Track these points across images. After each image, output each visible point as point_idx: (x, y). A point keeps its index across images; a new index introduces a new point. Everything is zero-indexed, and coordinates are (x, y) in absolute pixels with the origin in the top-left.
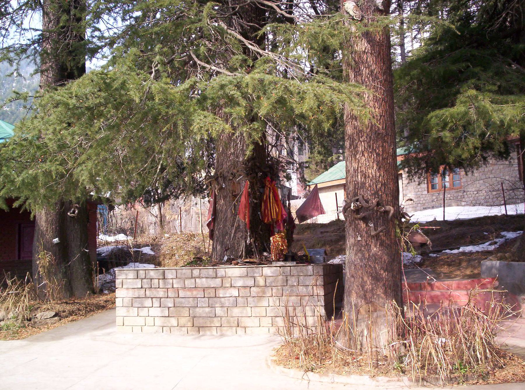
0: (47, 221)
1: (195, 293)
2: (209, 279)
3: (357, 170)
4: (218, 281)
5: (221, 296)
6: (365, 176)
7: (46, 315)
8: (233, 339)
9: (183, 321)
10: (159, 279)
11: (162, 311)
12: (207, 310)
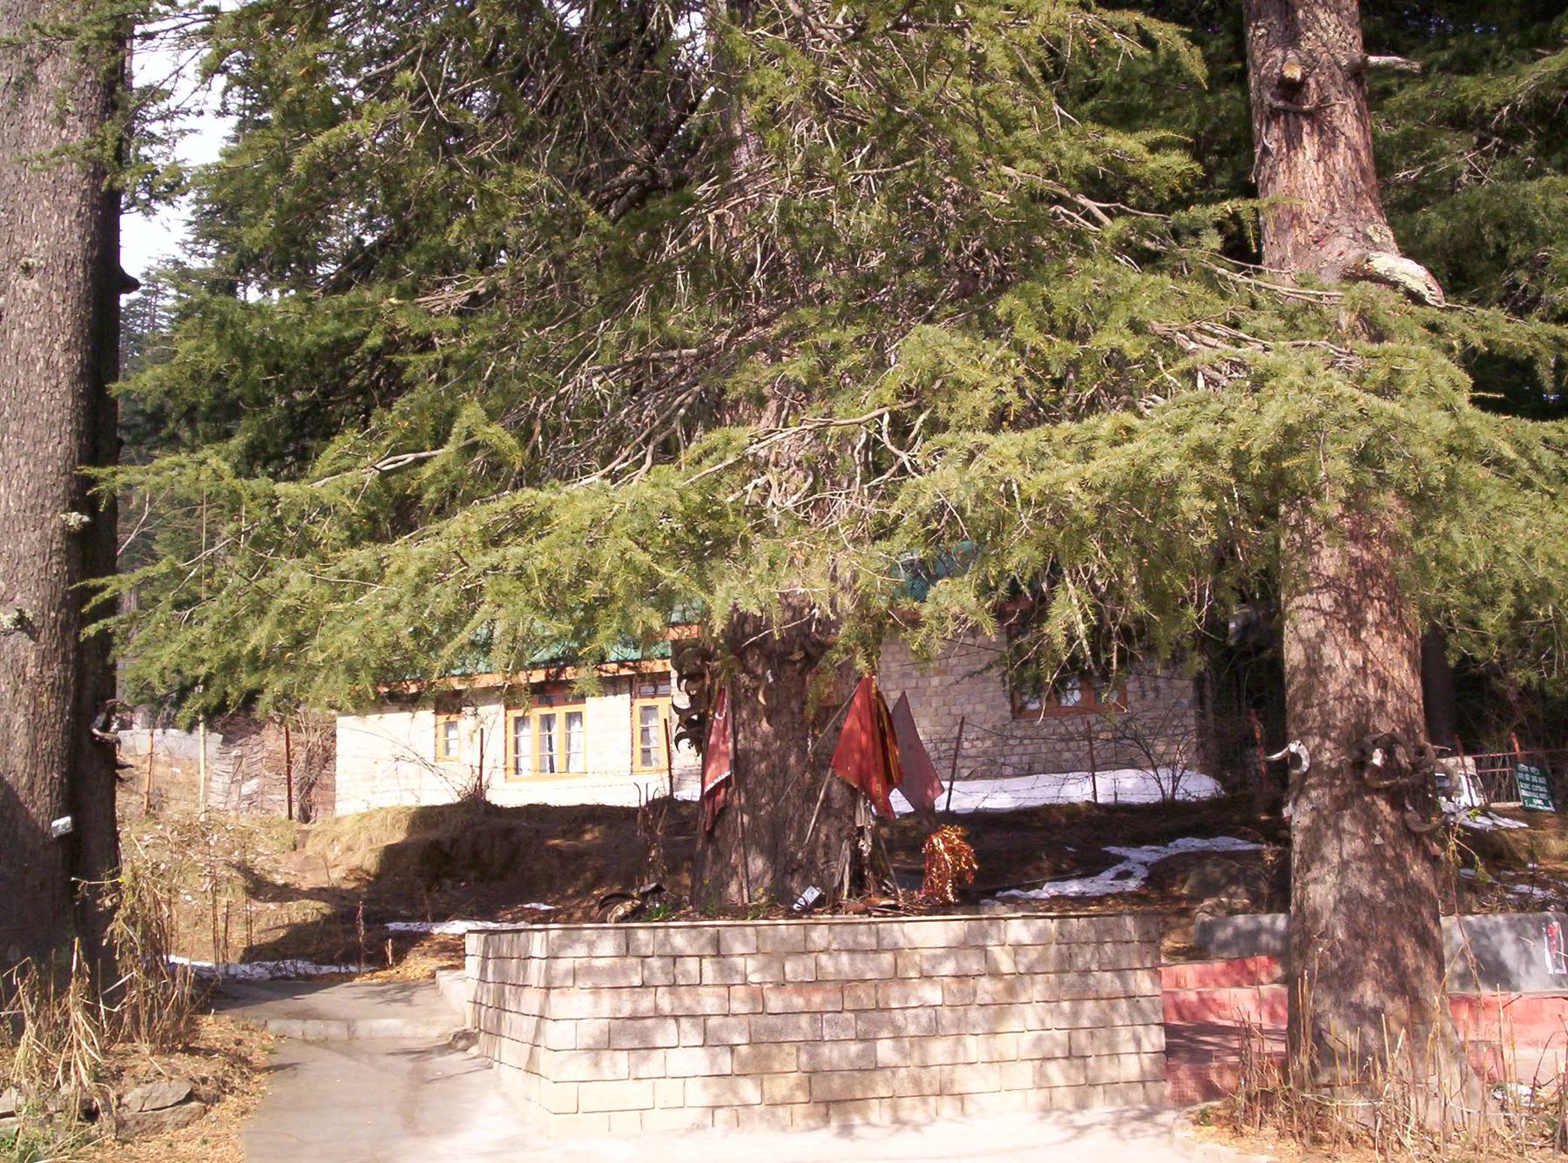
1: (817, 999)
2: (859, 957)
3: (1364, 668)
4: (887, 958)
5: (894, 1005)
6: (1383, 684)
8: (943, 1131)
9: (780, 1087)
11: (713, 1060)
12: (854, 1048)
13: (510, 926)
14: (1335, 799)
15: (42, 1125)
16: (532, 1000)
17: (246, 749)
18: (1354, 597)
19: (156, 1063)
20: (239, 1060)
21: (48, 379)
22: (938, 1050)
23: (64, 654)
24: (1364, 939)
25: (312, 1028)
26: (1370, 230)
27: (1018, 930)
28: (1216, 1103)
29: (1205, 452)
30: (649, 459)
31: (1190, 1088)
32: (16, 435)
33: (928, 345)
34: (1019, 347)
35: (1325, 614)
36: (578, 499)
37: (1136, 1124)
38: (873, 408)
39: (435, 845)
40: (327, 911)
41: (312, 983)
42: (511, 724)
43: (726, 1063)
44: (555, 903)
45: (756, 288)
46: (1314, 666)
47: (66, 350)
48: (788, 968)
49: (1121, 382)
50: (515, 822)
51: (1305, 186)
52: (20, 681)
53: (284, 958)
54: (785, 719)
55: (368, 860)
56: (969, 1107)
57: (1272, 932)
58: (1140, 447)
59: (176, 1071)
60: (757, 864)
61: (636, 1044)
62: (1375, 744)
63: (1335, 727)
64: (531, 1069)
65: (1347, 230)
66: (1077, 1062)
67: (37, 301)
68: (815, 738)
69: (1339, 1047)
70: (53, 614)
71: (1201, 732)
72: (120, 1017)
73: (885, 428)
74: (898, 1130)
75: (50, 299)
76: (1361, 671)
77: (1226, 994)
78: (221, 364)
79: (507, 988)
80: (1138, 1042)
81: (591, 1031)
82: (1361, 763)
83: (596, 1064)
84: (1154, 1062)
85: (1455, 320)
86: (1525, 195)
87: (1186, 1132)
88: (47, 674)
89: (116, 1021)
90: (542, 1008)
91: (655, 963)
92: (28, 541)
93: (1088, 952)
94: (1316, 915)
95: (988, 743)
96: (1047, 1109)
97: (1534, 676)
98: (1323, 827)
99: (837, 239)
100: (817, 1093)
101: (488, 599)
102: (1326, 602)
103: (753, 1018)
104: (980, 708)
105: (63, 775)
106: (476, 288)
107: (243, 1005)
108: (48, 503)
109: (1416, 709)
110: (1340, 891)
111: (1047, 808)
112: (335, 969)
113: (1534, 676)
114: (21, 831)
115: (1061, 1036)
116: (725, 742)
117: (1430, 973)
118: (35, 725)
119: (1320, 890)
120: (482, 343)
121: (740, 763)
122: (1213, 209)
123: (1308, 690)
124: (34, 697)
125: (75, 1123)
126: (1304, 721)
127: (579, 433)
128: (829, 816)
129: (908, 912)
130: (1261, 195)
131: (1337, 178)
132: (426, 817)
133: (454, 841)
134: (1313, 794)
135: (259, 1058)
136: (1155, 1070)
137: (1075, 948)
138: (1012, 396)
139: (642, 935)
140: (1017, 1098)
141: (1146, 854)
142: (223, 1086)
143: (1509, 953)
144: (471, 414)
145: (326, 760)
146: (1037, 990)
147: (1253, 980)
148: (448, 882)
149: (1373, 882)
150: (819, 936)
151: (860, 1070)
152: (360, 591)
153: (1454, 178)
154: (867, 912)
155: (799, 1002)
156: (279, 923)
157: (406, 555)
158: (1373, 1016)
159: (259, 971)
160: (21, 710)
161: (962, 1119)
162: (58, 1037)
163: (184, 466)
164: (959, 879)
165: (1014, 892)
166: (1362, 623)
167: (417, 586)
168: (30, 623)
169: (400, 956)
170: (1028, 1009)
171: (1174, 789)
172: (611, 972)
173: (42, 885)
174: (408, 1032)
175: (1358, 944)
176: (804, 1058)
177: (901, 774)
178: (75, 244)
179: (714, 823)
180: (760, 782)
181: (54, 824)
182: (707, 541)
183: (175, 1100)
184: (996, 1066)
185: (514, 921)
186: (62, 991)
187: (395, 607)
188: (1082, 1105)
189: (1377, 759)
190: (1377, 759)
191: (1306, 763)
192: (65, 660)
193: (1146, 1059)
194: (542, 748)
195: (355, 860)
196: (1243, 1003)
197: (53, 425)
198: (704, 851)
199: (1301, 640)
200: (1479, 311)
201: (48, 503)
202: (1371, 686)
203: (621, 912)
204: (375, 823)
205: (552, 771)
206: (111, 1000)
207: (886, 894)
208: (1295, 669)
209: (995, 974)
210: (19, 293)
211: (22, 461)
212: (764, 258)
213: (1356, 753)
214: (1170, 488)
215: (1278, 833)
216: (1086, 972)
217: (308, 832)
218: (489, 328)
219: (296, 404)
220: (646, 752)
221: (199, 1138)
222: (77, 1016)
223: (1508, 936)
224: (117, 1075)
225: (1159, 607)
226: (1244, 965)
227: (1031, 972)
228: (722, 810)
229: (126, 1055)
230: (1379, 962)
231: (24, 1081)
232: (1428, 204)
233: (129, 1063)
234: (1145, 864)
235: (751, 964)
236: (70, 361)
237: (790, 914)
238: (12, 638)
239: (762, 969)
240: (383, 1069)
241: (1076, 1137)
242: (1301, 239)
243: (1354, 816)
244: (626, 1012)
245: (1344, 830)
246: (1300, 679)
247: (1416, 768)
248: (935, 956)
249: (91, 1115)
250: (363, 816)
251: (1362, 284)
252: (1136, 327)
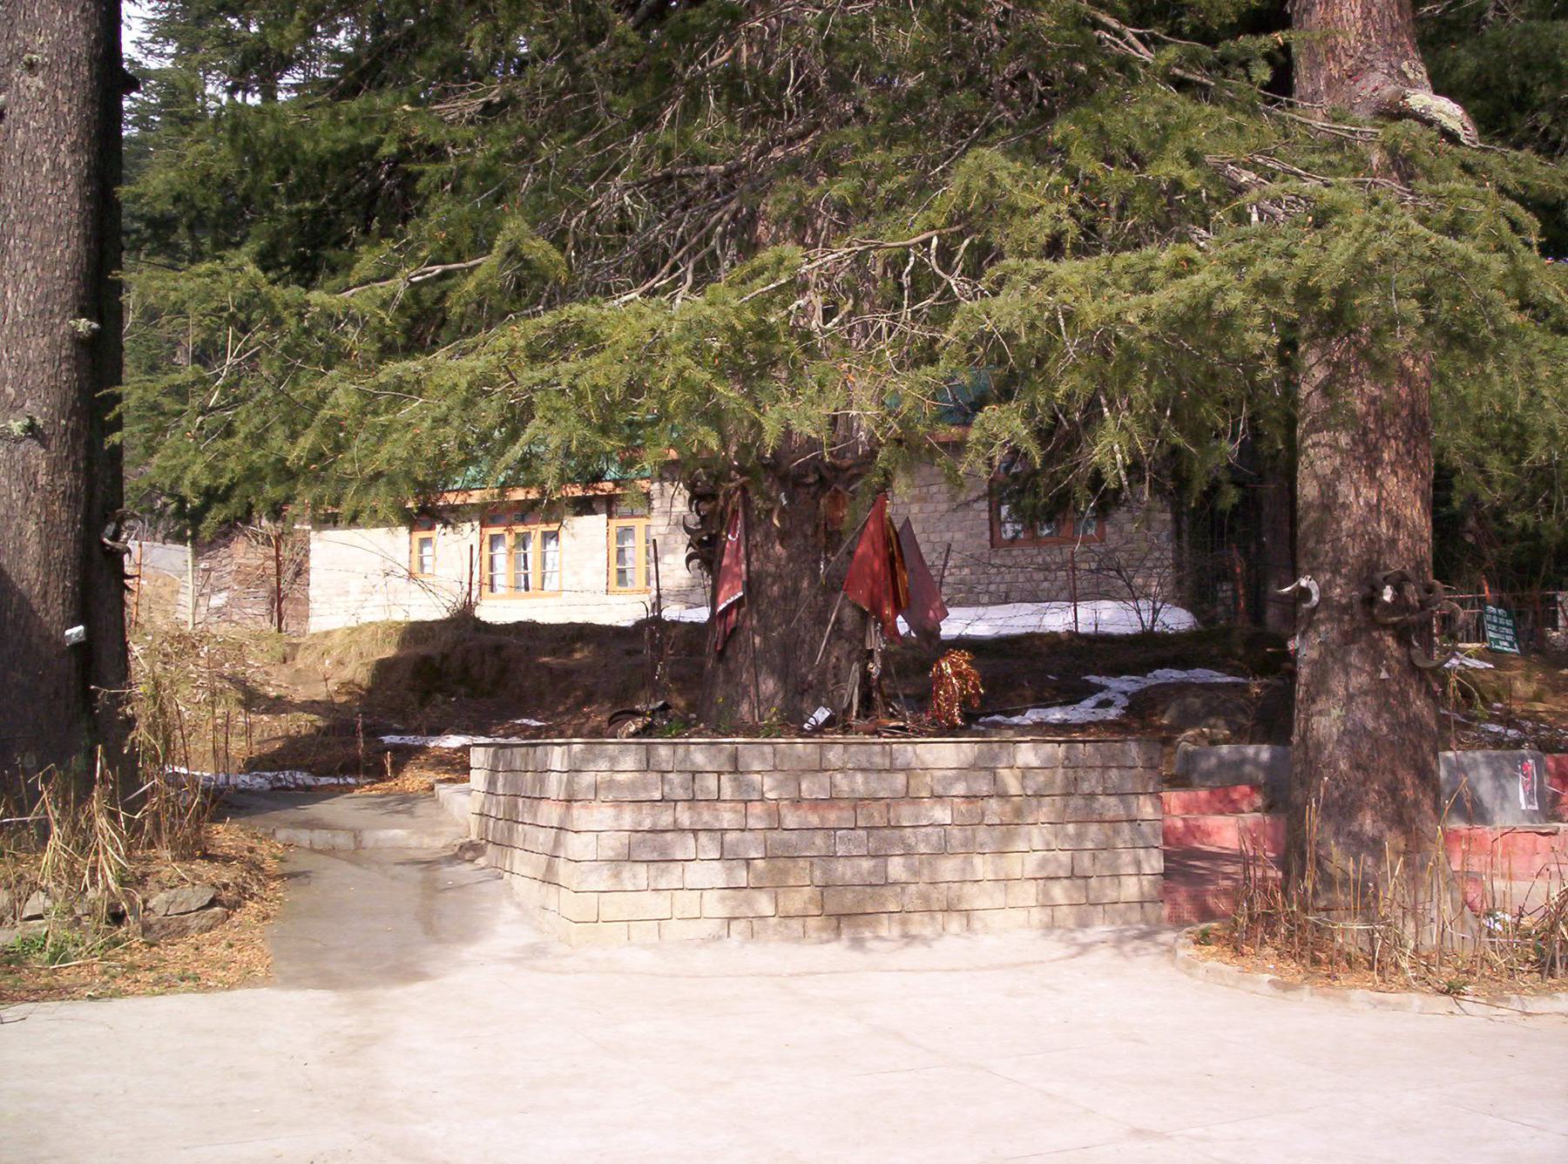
0: (45, 561)
1: (832, 817)
2: (873, 776)
4: (900, 780)
6: (1396, 523)
7: (186, 901)
8: (952, 944)
9: (798, 900)
10: (720, 773)
12: (866, 864)
13: (502, 741)
14: (1344, 634)
15: (70, 928)
16: (550, 813)
17: (215, 563)
18: (1372, 436)
19: (179, 869)
20: (254, 867)
21: (54, 181)
22: (948, 868)
23: (75, 463)
24: (1365, 769)
25: (320, 837)
26: (1405, 66)
27: (1027, 754)
28: (1215, 925)
29: (1269, 287)
30: (690, 277)
31: (1186, 910)
32: (23, 238)
33: (989, 164)
34: (1071, 173)
35: (1342, 451)
36: (625, 315)
37: (1137, 942)
38: (923, 231)
39: (426, 659)
40: (320, 723)
41: (313, 794)
42: (487, 540)
43: (742, 877)
44: (546, 720)
45: (789, 106)
46: (1329, 504)
47: (73, 152)
48: (804, 786)
49: (1172, 214)
50: (505, 639)
51: (1341, 19)
52: (31, 489)
53: (282, 769)
54: (799, 541)
55: (357, 671)
56: (977, 925)
57: (1255, 762)
58: (1203, 279)
59: (198, 877)
60: (769, 685)
61: (655, 856)
62: (1386, 580)
63: (1347, 563)
64: (549, 879)
65: (1382, 65)
66: (1080, 882)
67: (42, 100)
68: (828, 561)
69: (1339, 875)
70: (63, 422)
71: (1178, 566)
72: (141, 824)
73: (933, 252)
74: (907, 944)
75: (55, 97)
76: (1374, 509)
77: (1213, 821)
78: (232, 168)
79: (520, 801)
80: (1138, 863)
81: (613, 843)
82: (1371, 599)
83: (617, 875)
84: (1154, 884)
85: (1493, 161)
86: (1557, 36)
87: (1187, 951)
88: (59, 482)
89: (135, 828)
90: (561, 820)
91: (674, 778)
92: (38, 346)
93: (1094, 776)
94: (1319, 747)
95: (966, 571)
96: (1050, 927)
97: (1530, 519)
98: (1329, 660)
99: (878, 58)
100: (830, 908)
101: (539, 414)
102: (1344, 440)
103: (769, 834)
104: (959, 536)
105: (74, 583)
106: (490, 97)
107: (248, 814)
108: (57, 309)
109: (1425, 549)
110: (1344, 724)
111: (1030, 637)
112: (334, 781)
113: (1530, 519)
114: (34, 640)
115: (1065, 857)
116: (738, 564)
117: (1427, 805)
118: (48, 534)
119: (1326, 721)
120: (500, 155)
121: (753, 586)
122: (1264, 39)
123: (1320, 528)
124: (45, 504)
125: (103, 926)
126: (1315, 557)
127: (611, 248)
128: (840, 638)
129: (920, 733)
130: (1296, 26)
131: (1374, 11)
132: (417, 632)
133: (445, 657)
134: (1322, 628)
135: (271, 865)
136: (1155, 893)
137: (1081, 773)
138: (1068, 223)
139: (664, 752)
140: (1021, 915)
141: (1125, 684)
142: (244, 894)
143: (1485, 788)
144: (514, 226)
145: (298, 574)
146: (1045, 812)
147: (1236, 810)
148: (439, 697)
149: (1377, 716)
150: (834, 755)
151: (871, 885)
152: (395, 403)
153: (1480, 14)
154: (875, 733)
155: (814, 820)
156: (273, 734)
157: (450, 367)
158: (1375, 847)
159: (259, 781)
160: (33, 518)
161: (967, 934)
162: (82, 841)
163: (219, 274)
164: (965, 702)
165: (997, 718)
166: (1378, 462)
167: (466, 399)
168: (40, 431)
169: (398, 768)
170: (1035, 830)
171: (1154, 621)
172: (632, 786)
173: (57, 693)
174: (413, 842)
175: (1360, 775)
176: (818, 873)
177: (908, 599)
178: (80, 42)
179: (725, 643)
180: (773, 603)
181: (68, 632)
182: (755, 356)
183: (199, 905)
184: (1001, 884)
185: (506, 736)
186: (84, 797)
187: (445, 421)
188: (1083, 924)
189: (1388, 595)
190: (1388, 595)
191: (1315, 598)
192: (75, 469)
193: (1145, 881)
194: (517, 567)
195: (347, 674)
196: (1226, 832)
197: (60, 228)
198: (715, 670)
199: (1316, 477)
200: (1513, 153)
201: (57, 309)
202: (1383, 523)
203: (632, 729)
204: (365, 637)
205: (527, 588)
206: (131, 808)
207: (892, 716)
208: (1309, 506)
209: (1004, 796)
210: (23, 91)
211: (29, 265)
212: (797, 75)
213: (1367, 590)
214: (1227, 322)
215: (1280, 665)
216: (1092, 795)
217: (297, 645)
218: (508, 138)
219: (326, 208)
220: (622, 572)
221: (224, 942)
222: (102, 822)
223: (1485, 772)
224: (141, 881)
225: (1196, 439)
226: (1227, 795)
227: (1038, 795)
228: (734, 630)
229: (149, 860)
230: (1379, 793)
231: (52, 884)
232: (1453, 42)
233: (153, 868)
234: (1125, 693)
235: (768, 782)
236: (76, 163)
237: (801, 733)
238: (22, 446)
239: (779, 786)
240: (393, 878)
241: (1080, 954)
242: (1335, 73)
243: (1361, 651)
244: (647, 825)
245: (1351, 665)
246: (1313, 515)
247: (1424, 605)
248: (945, 777)
249: (117, 918)
250: (353, 630)
251: (1407, 121)
252: (1193, 158)
